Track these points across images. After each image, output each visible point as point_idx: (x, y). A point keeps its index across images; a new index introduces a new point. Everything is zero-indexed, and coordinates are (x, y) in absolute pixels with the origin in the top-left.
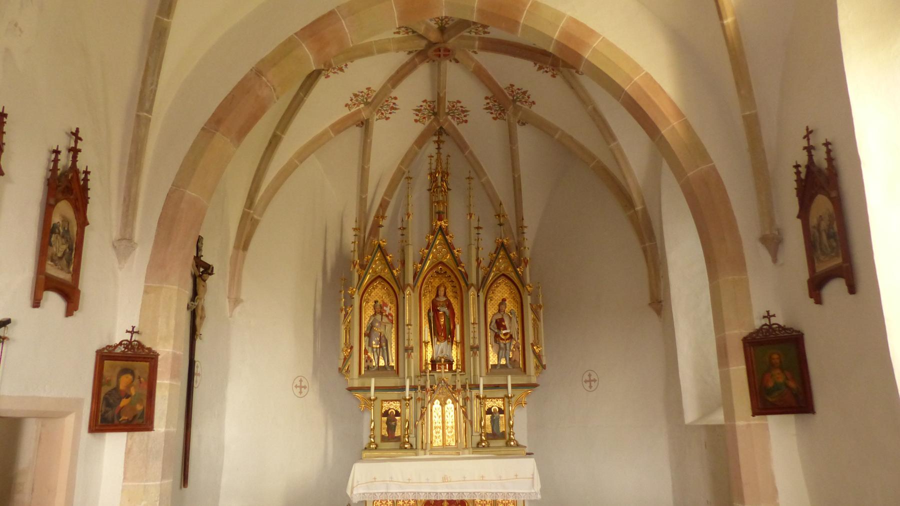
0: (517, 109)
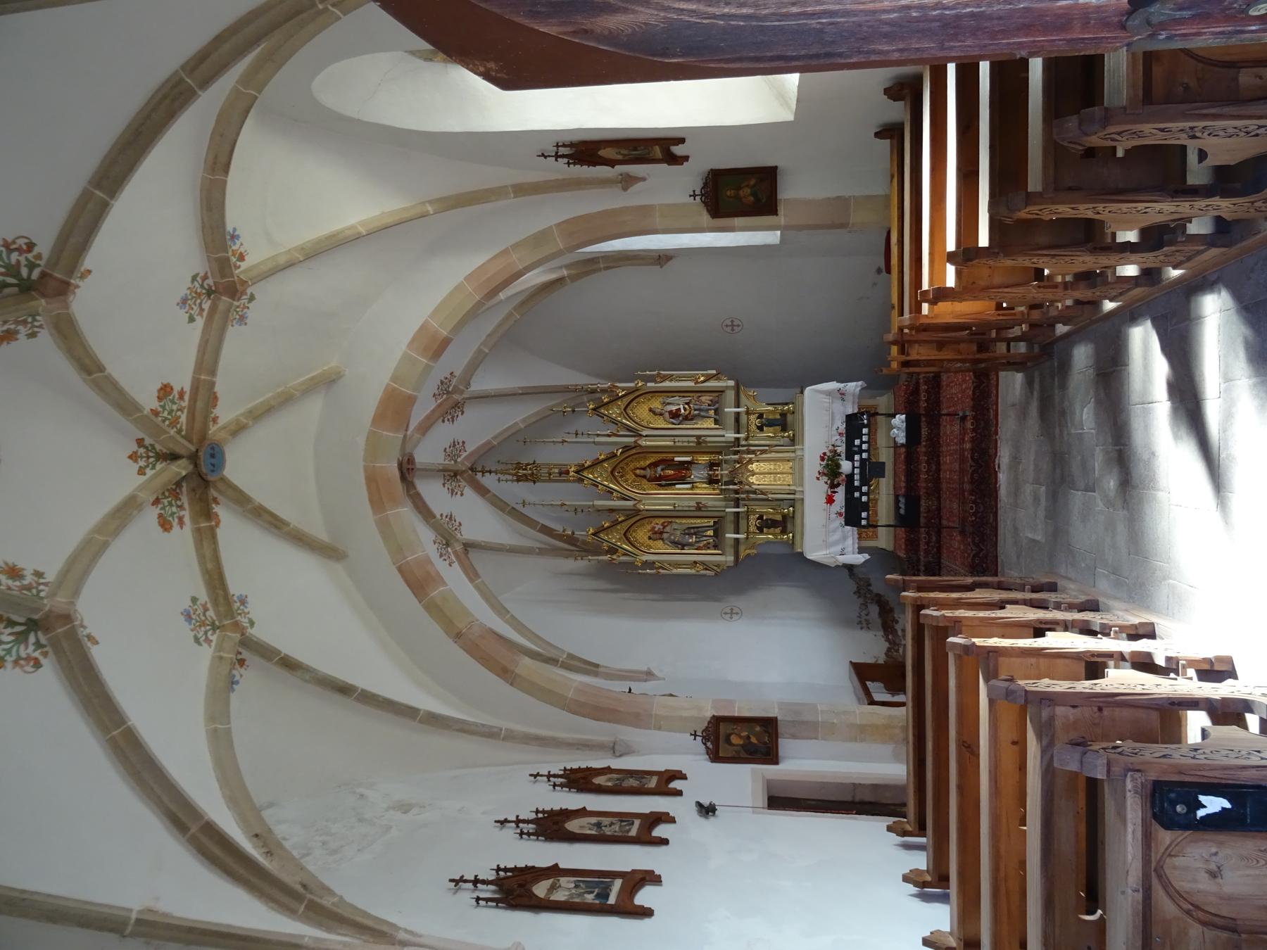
0: (457, 390)
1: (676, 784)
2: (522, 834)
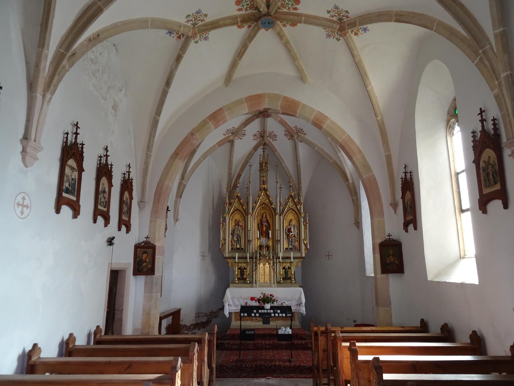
0: (298, 136)
1: (124, 228)
2: (101, 157)
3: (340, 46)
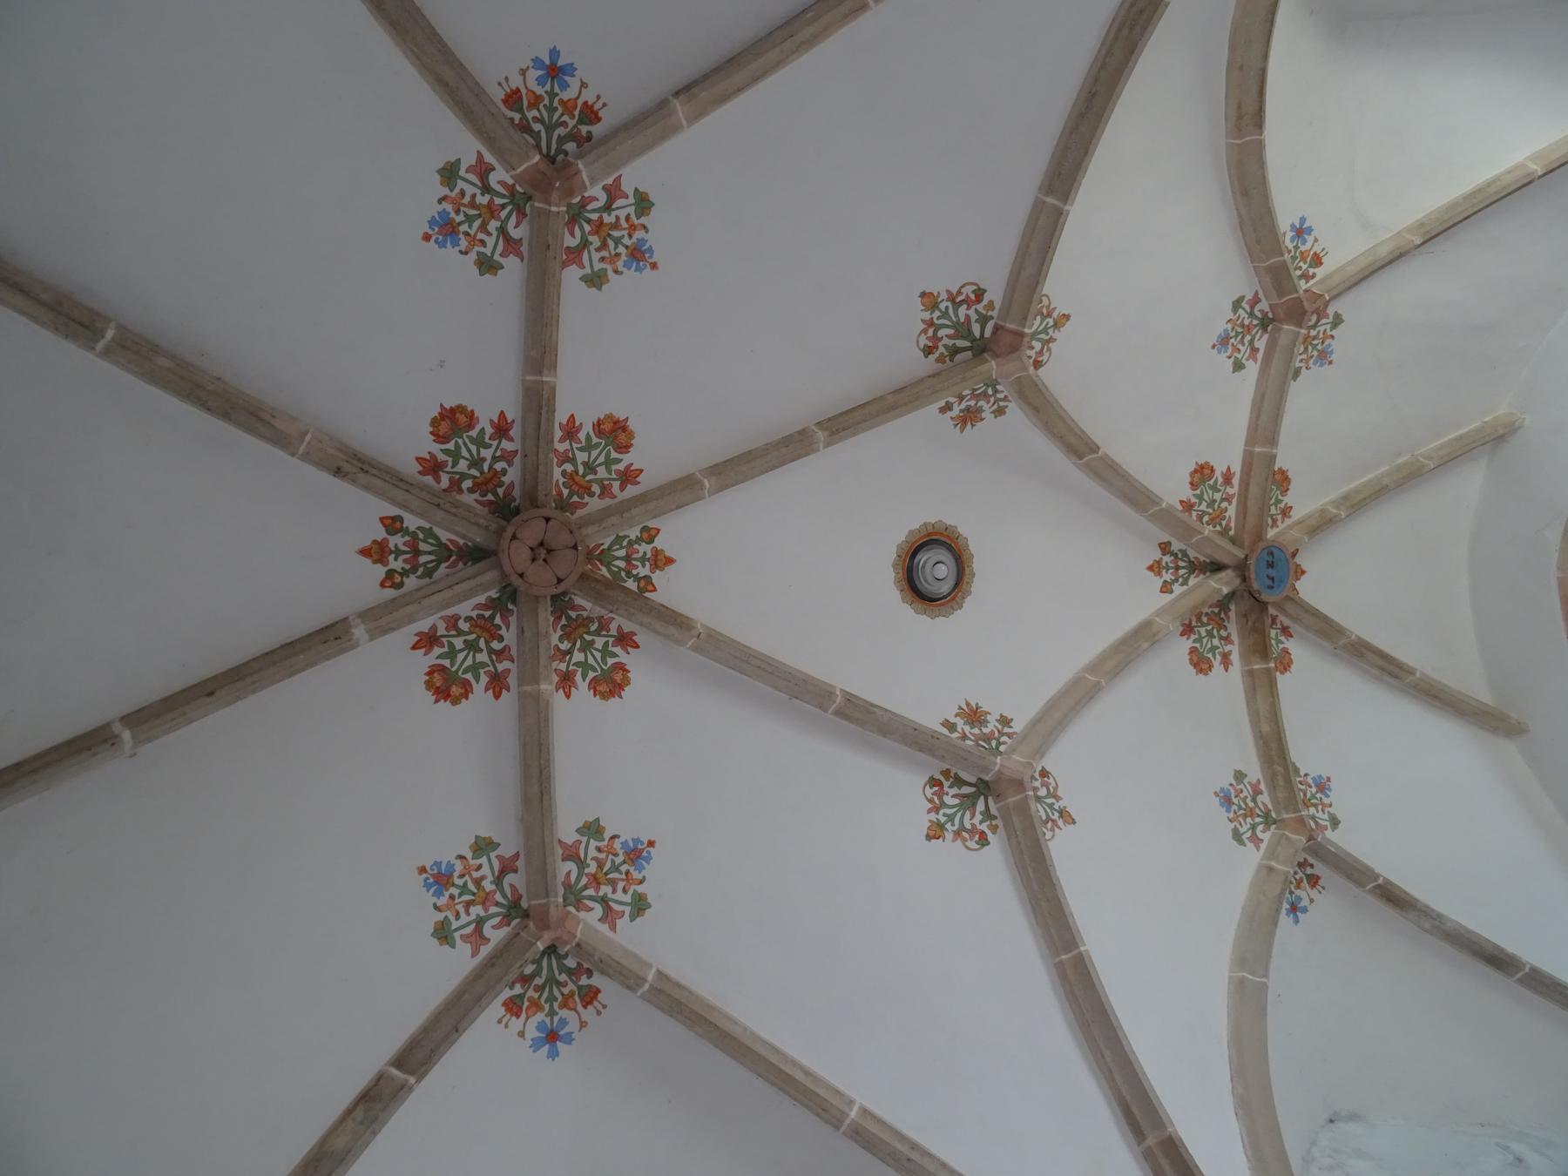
3: (1361, 315)
